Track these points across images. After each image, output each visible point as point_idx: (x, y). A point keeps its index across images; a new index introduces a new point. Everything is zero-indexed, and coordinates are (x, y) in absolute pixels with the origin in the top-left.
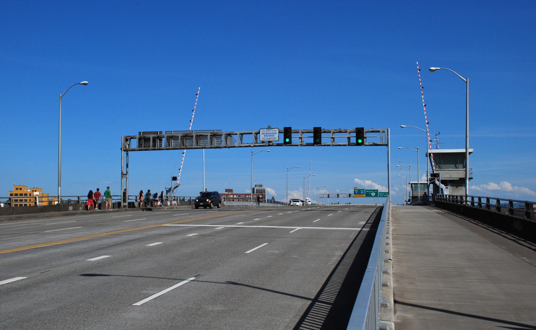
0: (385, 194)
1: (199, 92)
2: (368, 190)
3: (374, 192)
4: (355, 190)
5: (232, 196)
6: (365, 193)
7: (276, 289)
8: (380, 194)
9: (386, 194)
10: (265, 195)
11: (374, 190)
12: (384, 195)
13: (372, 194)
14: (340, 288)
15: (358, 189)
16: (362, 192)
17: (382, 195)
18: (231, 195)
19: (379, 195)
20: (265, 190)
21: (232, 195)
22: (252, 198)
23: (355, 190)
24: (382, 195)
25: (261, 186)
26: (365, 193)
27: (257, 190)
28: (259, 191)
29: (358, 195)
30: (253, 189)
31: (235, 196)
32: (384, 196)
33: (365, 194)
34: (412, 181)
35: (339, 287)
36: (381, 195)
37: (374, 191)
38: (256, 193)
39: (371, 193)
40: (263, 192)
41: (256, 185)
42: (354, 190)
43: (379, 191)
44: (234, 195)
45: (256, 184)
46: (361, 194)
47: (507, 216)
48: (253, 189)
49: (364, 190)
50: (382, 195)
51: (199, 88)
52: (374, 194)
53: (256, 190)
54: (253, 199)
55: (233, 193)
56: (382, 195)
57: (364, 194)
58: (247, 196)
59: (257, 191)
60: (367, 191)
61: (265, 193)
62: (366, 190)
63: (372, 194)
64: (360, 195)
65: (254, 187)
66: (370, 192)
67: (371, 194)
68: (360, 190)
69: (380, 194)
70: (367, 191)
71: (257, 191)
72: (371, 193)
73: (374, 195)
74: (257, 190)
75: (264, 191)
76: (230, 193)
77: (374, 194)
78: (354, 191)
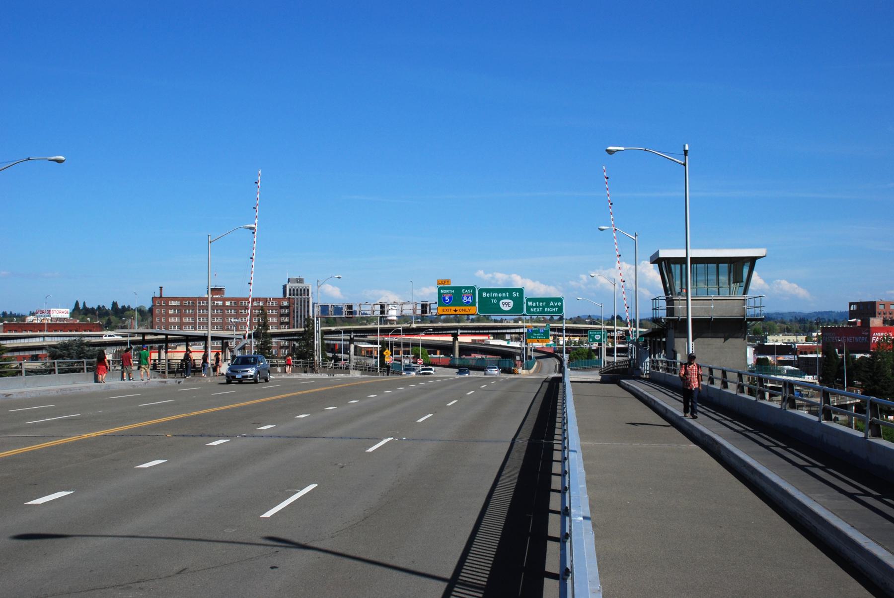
0: (547, 306)
1: (259, 178)
2: (488, 291)
3: (511, 297)
4: (442, 291)
5: (220, 303)
6: (477, 300)
7: (304, 541)
8: (530, 303)
9: (552, 303)
10: (308, 299)
11: (510, 291)
12: (543, 307)
13: (597, 337)
14: (469, 558)
15: (452, 285)
16: (465, 298)
17: (539, 307)
18: (218, 301)
19: (528, 308)
20: (308, 290)
21: (220, 301)
22: (211, 306)
23: (442, 291)
24: (536, 307)
25: (300, 281)
26: (477, 300)
27: (292, 290)
28: (295, 292)
29: (454, 308)
30: (285, 287)
31: (228, 303)
32: (546, 310)
33: (477, 305)
34: (696, 247)
35: (470, 556)
36: (533, 307)
37: (511, 295)
38: (290, 295)
39: (499, 299)
40: (304, 293)
41: (289, 279)
42: (440, 289)
43: (526, 295)
44: (224, 300)
45: (290, 277)
46: (463, 305)
47: (658, 329)
48: (285, 287)
49: (473, 288)
50: (539, 307)
51: (260, 172)
52: (598, 337)
53: (290, 290)
54: (214, 310)
55: (224, 297)
56: (536, 307)
57: (473, 304)
58: (255, 303)
59: (292, 292)
60: (484, 294)
61: (308, 295)
62: (481, 291)
63: (597, 337)
64: (457, 308)
65: (286, 282)
66: (494, 298)
67: (594, 336)
68: (458, 289)
69: (530, 303)
70: (484, 294)
71: (292, 292)
72: (498, 302)
73: (598, 339)
74: (292, 290)
75: (306, 291)
76: (217, 296)
77: (508, 304)
78: (439, 293)
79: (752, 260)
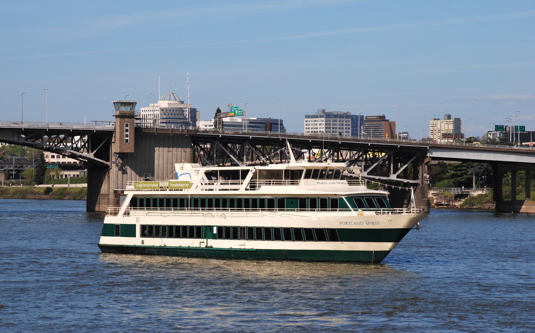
39: (236, 110)
69: (239, 111)
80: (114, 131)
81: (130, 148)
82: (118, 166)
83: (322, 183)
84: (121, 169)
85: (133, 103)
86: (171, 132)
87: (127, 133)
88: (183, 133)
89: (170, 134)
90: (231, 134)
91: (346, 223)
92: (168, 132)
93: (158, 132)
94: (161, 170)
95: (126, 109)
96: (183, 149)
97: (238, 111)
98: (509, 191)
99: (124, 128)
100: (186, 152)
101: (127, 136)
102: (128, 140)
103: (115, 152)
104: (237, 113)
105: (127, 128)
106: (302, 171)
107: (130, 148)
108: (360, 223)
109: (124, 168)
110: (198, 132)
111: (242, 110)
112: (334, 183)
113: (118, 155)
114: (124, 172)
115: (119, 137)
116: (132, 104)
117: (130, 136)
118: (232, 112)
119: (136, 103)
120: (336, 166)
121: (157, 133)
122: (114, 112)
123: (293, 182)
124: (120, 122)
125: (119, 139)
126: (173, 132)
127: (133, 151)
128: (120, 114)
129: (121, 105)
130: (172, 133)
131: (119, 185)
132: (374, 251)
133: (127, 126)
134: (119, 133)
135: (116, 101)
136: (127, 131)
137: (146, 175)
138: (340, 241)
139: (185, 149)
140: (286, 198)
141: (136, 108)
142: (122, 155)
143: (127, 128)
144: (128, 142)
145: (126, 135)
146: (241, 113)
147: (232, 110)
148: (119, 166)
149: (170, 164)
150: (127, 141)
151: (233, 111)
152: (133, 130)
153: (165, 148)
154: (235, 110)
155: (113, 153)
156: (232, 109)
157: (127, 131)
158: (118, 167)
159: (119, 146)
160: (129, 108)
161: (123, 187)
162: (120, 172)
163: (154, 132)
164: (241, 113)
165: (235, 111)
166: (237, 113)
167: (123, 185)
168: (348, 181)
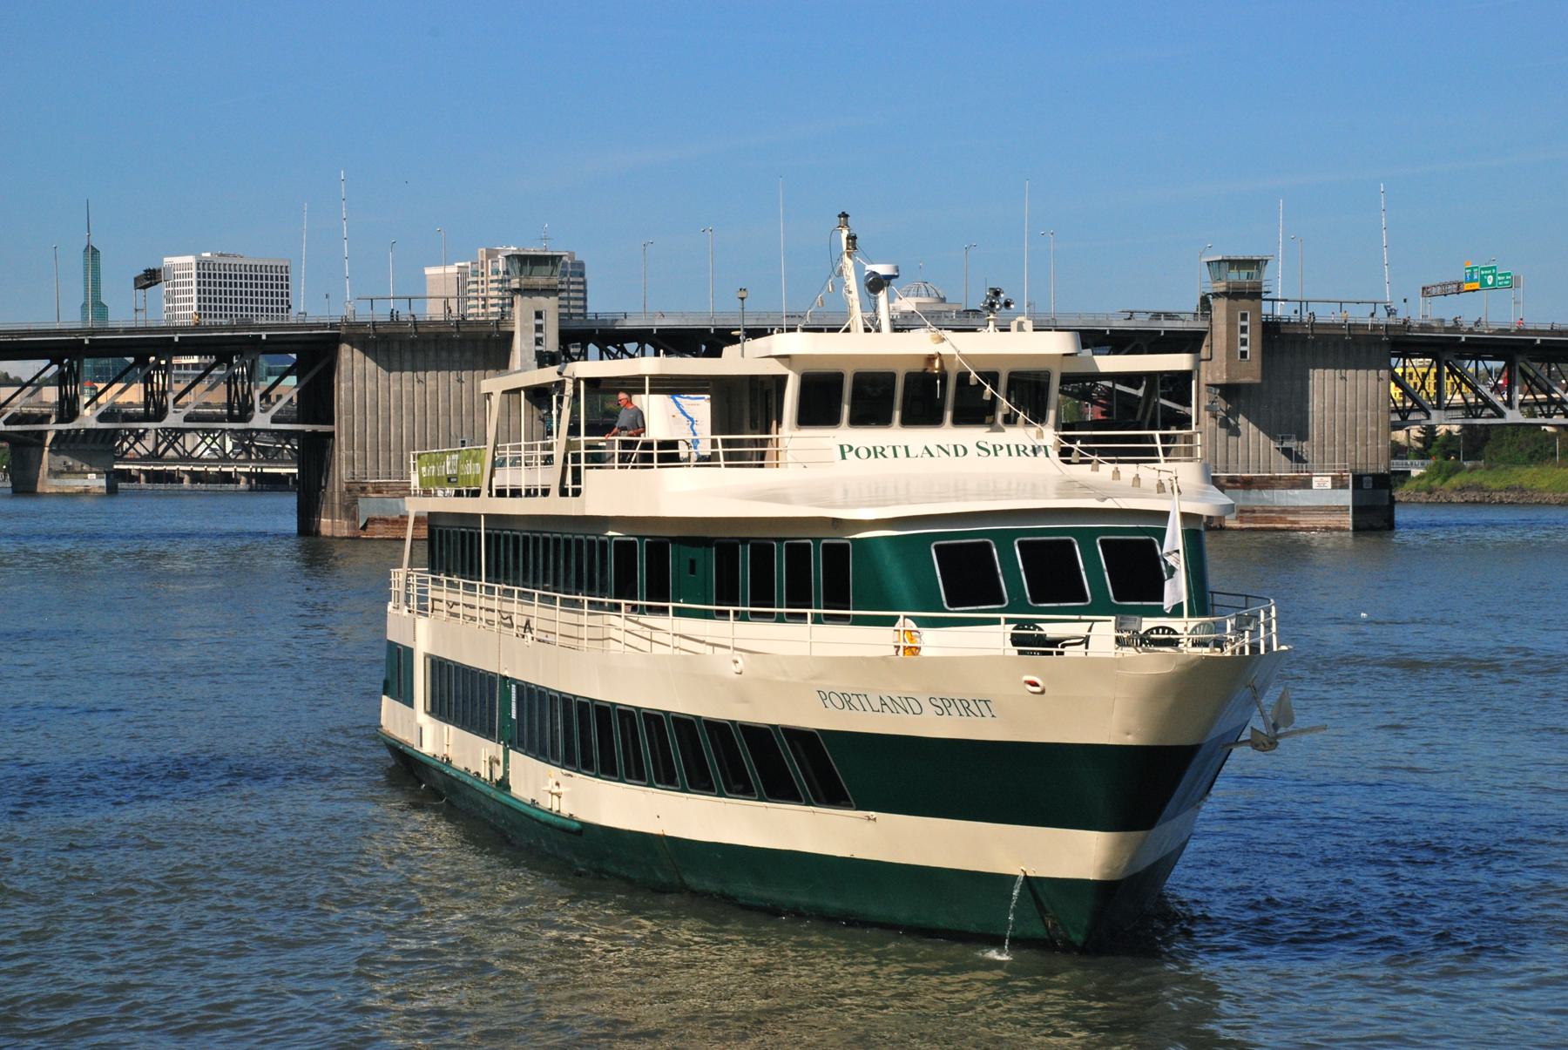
39: (1488, 275)
69: (1499, 278)
79: (1267, 261)
80: (1206, 332)
81: (1250, 373)
82: (1215, 417)
83: (874, 452)
84: (1224, 423)
85: (1258, 261)
86: (1347, 332)
87: (1244, 336)
88: (1375, 333)
89: (1345, 335)
90: (1489, 334)
91: (846, 701)
92: (1339, 332)
93: (1316, 331)
94: (1318, 426)
95: (1238, 277)
96: (1338, 372)
97: (1494, 278)
98: (373, 663)
99: (1236, 324)
100: (1345, 378)
101: (1244, 342)
102: (1246, 352)
103: (1210, 381)
104: (1490, 283)
105: (1244, 323)
106: (781, 381)
107: (1250, 373)
108: (906, 704)
109: (1232, 421)
110: (1408, 331)
111: (1509, 274)
112: (959, 451)
113: (1218, 391)
114: (1234, 431)
115: (1224, 345)
116: (1255, 264)
117: (1252, 345)
118: (1472, 280)
119: (1267, 261)
120: (964, 352)
121: (1312, 334)
122: (1209, 285)
123: (740, 443)
124: (1229, 310)
125: (1224, 351)
126: (1352, 332)
127: (1258, 381)
128: (1228, 288)
129: (1231, 268)
130: (1350, 335)
131: (1218, 465)
132: (1026, 877)
133: (1244, 317)
134: (1224, 335)
135: (1220, 258)
136: (1244, 329)
137: (1282, 438)
138: (858, 808)
139: (1343, 371)
140: (675, 540)
141: (1267, 273)
142: (1229, 391)
143: (1244, 323)
144: (1246, 357)
145: (1241, 339)
146: (1507, 282)
147: (1471, 277)
148: (1219, 418)
149: (1340, 410)
150: (1244, 354)
151: (1475, 277)
152: (1259, 329)
153: (1326, 371)
154: (1482, 276)
155: (1203, 387)
156: (1472, 273)
157: (1244, 329)
158: (1216, 418)
159: (1224, 367)
160: (1244, 274)
161: (1227, 468)
162: (1222, 432)
163: (1305, 331)
164: (1507, 282)
165: (1482, 276)
166: (1490, 283)
167: (1227, 461)
168: (726, 443)
